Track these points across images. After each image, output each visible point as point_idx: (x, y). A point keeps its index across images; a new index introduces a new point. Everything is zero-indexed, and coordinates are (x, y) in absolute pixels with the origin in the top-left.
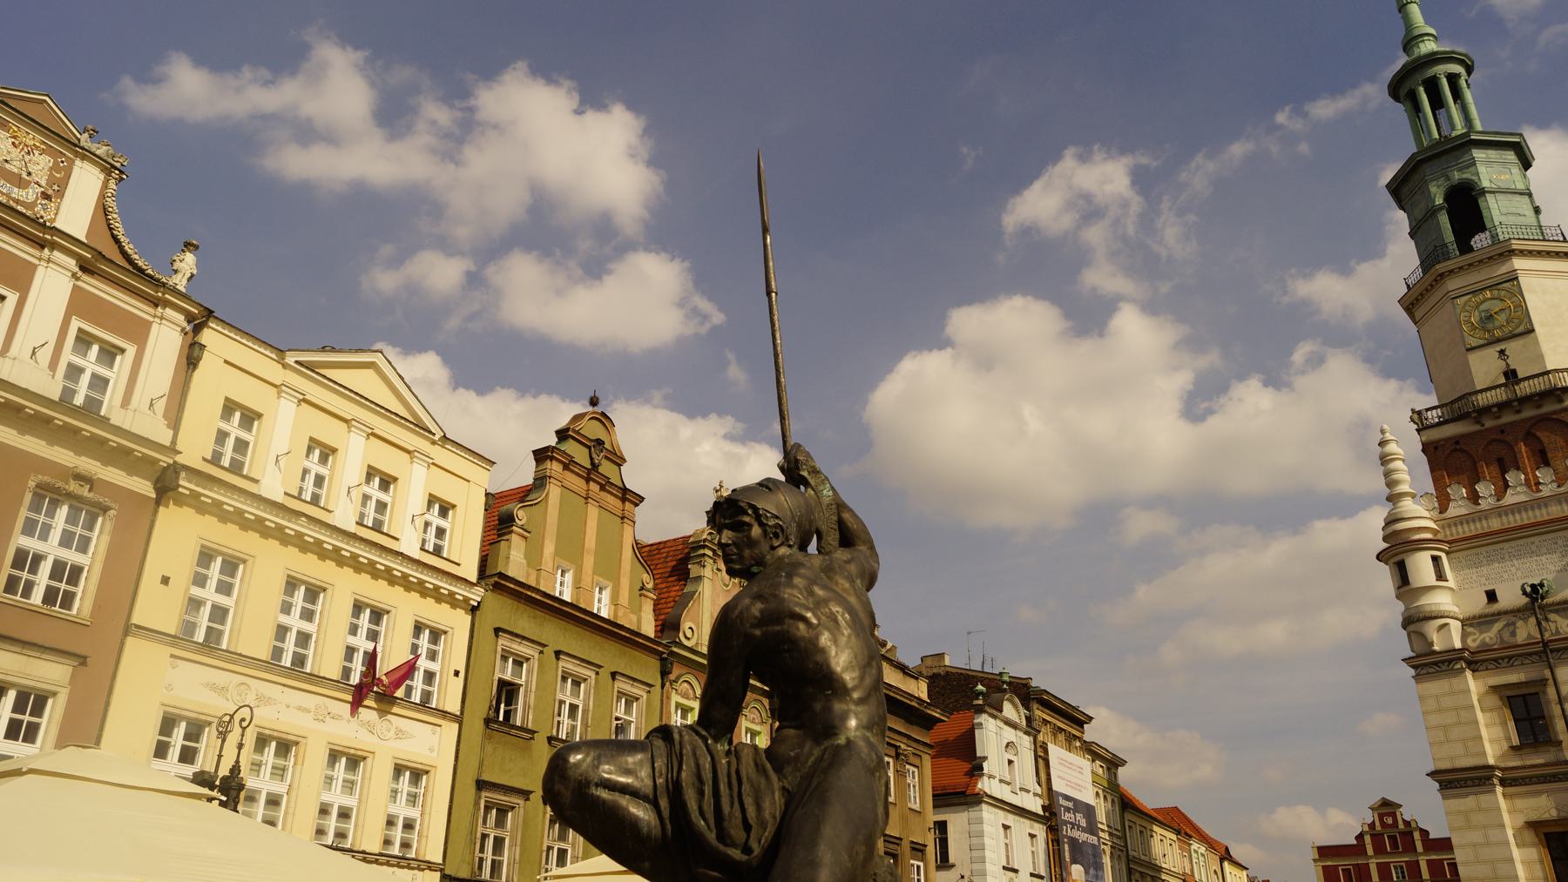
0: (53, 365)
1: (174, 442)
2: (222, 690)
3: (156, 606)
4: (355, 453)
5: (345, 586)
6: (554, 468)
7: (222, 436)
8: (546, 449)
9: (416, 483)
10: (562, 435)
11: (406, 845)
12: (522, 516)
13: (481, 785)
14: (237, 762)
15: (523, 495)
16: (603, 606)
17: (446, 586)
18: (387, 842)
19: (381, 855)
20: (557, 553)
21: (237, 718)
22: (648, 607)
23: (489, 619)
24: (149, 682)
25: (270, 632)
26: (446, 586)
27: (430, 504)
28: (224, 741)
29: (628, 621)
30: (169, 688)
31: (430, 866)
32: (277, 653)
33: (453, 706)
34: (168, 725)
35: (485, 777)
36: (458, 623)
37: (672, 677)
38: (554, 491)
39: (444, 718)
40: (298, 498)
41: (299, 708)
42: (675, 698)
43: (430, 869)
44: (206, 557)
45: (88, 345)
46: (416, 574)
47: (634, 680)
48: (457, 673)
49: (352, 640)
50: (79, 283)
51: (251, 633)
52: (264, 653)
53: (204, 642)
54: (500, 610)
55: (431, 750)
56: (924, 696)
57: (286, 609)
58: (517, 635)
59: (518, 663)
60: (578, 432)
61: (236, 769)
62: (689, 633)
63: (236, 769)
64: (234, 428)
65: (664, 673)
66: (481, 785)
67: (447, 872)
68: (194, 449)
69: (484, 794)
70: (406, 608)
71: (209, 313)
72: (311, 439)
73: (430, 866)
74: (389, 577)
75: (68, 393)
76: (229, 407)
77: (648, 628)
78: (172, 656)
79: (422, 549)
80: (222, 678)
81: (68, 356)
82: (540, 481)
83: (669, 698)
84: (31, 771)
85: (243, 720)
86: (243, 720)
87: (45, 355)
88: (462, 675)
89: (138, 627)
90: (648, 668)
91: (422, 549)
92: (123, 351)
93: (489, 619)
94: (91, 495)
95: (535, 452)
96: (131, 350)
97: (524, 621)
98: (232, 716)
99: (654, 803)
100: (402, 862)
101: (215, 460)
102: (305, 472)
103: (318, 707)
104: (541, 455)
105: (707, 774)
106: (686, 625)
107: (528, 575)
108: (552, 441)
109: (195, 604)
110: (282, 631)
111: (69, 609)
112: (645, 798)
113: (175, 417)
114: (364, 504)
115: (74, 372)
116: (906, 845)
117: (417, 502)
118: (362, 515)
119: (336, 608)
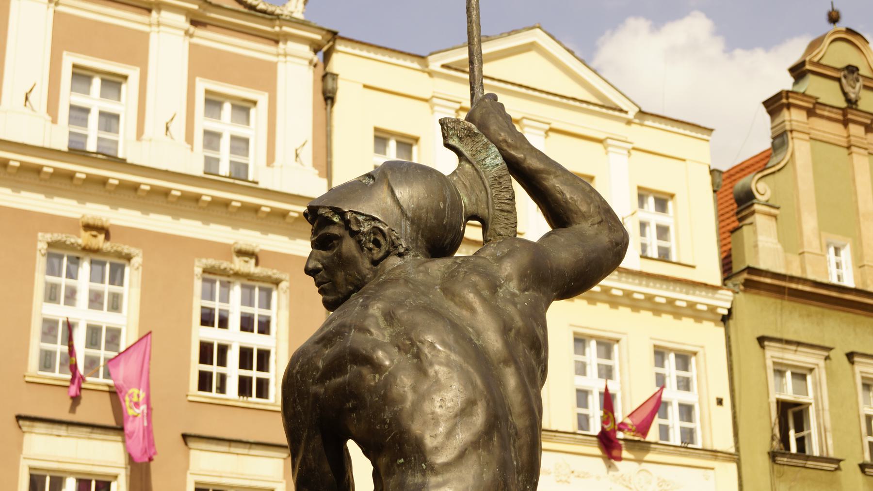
0: (189, 138)
12: (763, 189)
15: (760, 164)
38: (800, 148)
45: (219, 104)
52: (571, 425)
71: (334, 35)
75: (211, 163)
81: (68, 97)
82: (780, 140)
88: (727, 402)
96: (262, 98)
108: (787, 83)
115: (79, 113)
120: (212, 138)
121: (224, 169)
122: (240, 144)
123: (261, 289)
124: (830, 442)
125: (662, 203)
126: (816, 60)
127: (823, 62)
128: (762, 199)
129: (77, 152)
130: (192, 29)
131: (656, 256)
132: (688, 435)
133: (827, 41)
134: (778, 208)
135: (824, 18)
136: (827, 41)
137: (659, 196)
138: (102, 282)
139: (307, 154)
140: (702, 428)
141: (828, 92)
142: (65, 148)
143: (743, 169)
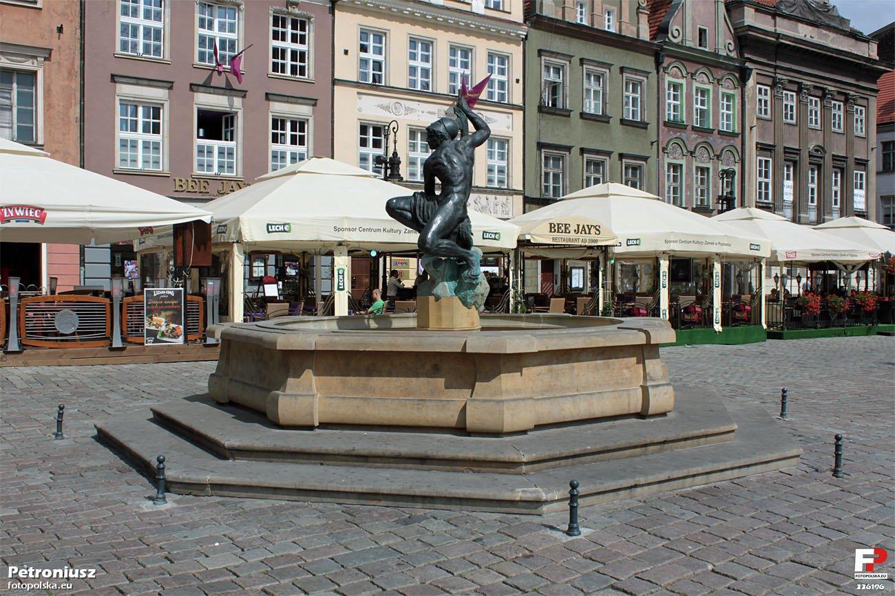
2: (387, 108)
3: (346, 68)
5: (443, 40)
11: (501, 182)
13: (541, 146)
14: (395, 149)
16: (610, 25)
17: (504, 29)
18: (490, 181)
19: (487, 188)
21: (391, 127)
22: (644, 20)
23: (534, 45)
24: (353, 108)
25: (406, 71)
26: (504, 29)
28: (387, 139)
29: (629, 32)
30: (360, 110)
31: (516, 192)
33: (518, 100)
34: (364, 129)
35: (542, 141)
36: (515, 52)
37: (665, 65)
39: (513, 109)
41: (429, 113)
42: (668, 79)
43: (516, 194)
44: (364, 34)
46: (485, 25)
47: (637, 70)
48: (518, 81)
49: (452, 69)
51: (397, 76)
53: (374, 83)
54: (540, 39)
55: (508, 128)
56: (874, 55)
57: (413, 57)
58: (553, 53)
59: (557, 70)
61: (395, 154)
62: (676, 34)
63: (395, 154)
65: (658, 64)
66: (541, 146)
67: (526, 195)
70: (482, 47)
73: (516, 192)
74: (468, 31)
77: (645, 35)
78: (358, 93)
79: (486, 7)
80: (385, 101)
83: (663, 79)
84: (299, 172)
85: (394, 128)
86: (394, 128)
88: (521, 81)
89: (339, 80)
90: (647, 63)
91: (486, 7)
93: (534, 45)
94: (299, 12)
97: (557, 43)
98: (389, 127)
99: (410, 212)
100: (499, 191)
103: (439, 110)
105: (422, 206)
106: (674, 27)
107: (556, 12)
109: (364, 62)
110: (413, 70)
111: (304, 75)
112: (409, 211)
116: (851, 162)
119: (441, 51)
131: (492, 7)
132: (377, 79)
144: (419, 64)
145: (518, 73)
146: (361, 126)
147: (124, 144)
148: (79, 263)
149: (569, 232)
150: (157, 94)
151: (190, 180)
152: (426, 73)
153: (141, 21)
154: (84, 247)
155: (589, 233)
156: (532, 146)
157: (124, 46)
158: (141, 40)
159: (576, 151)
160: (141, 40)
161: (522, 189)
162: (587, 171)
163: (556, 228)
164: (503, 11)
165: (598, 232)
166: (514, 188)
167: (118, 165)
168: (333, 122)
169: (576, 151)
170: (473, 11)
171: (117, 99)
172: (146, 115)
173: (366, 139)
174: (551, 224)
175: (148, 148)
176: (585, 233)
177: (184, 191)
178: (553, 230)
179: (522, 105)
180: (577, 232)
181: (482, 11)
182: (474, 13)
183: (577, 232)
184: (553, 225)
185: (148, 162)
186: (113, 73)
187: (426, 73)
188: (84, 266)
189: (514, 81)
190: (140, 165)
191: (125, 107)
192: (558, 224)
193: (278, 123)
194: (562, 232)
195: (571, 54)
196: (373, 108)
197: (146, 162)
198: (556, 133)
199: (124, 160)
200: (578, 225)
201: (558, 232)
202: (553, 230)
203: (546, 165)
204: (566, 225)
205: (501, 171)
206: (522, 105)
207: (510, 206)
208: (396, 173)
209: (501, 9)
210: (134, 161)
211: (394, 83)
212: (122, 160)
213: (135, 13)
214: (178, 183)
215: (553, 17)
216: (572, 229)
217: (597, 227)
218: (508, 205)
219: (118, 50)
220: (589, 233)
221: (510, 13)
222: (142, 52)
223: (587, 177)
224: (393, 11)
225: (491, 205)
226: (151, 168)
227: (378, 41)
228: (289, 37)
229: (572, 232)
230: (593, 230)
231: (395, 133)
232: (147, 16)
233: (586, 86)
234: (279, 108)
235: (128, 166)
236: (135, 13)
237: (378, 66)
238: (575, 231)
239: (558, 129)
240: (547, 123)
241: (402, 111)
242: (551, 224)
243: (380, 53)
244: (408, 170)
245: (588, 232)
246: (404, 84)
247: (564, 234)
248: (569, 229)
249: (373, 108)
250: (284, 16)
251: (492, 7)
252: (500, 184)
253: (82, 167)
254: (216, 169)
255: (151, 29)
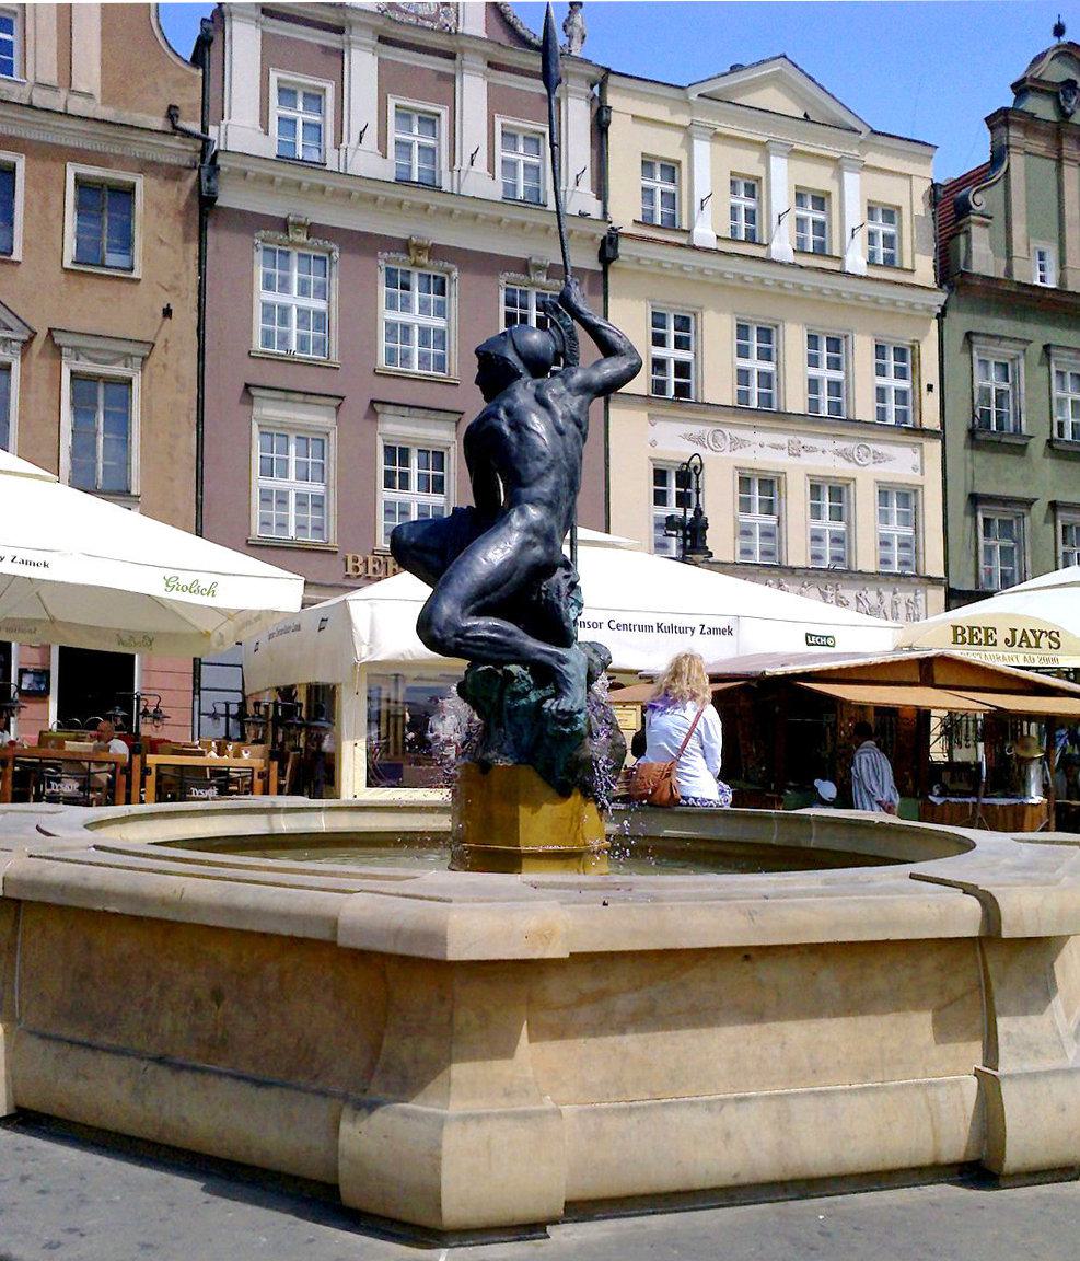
0: (491, 168)
1: (605, 213)
4: (782, 177)
6: (1015, 135)
7: (648, 193)
8: (1004, 111)
9: (854, 193)
10: (1021, 89)
12: (980, 200)
13: (975, 500)
15: (979, 178)
20: (1029, 235)
21: (692, 466)
27: (871, 210)
32: (744, 396)
33: (931, 420)
34: (660, 476)
38: (1016, 162)
40: (734, 240)
45: (409, 117)
48: (930, 388)
50: (491, 80)
52: (729, 398)
57: (743, 352)
60: (1038, 80)
64: (659, 185)
67: (951, 586)
68: (625, 210)
69: (980, 507)
71: (608, 71)
72: (732, 174)
75: (510, 188)
76: (648, 164)
81: (276, 110)
82: (999, 156)
87: (482, 157)
88: (936, 388)
92: (438, 115)
95: (986, 119)
96: (330, 88)
101: (647, 221)
102: (734, 209)
104: (998, 121)
108: (1008, 100)
110: (743, 376)
113: (601, 191)
114: (734, 217)
115: (287, 124)
117: (854, 213)
118: (872, 255)
120: (509, 166)
121: (521, 194)
122: (429, 153)
123: (420, 275)
124: (1023, 422)
125: (751, 191)
126: (1036, 76)
127: (1043, 78)
128: (978, 209)
129: (403, 181)
130: (489, 70)
131: (882, 262)
132: (682, 390)
133: (1049, 56)
134: (990, 218)
135: (1050, 30)
136: (1049, 56)
137: (885, 208)
138: (274, 268)
139: (587, 179)
140: (696, 384)
141: (1042, 108)
142: (500, 199)
143: (966, 180)
144: (754, 364)
145: (930, 373)
146: (655, 470)
147: (266, 498)
148: (192, 688)
149: (995, 644)
150: (317, 417)
151: (371, 558)
152: (835, 387)
153: (293, 300)
154: (201, 663)
155: (1038, 646)
156: (959, 501)
157: (268, 338)
158: (294, 331)
159: (1039, 510)
160: (294, 331)
161: (943, 576)
162: (1064, 543)
163: (967, 635)
164: (901, 269)
165: (1055, 645)
166: (928, 573)
167: (256, 531)
168: (607, 465)
169: (1039, 510)
170: (847, 270)
171: (255, 425)
172: (423, 464)
173: (665, 492)
174: (955, 628)
175: (269, 501)
176: (1029, 646)
177: (359, 576)
178: (960, 639)
179: (939, 429)
180: (1010, 643)
181: (863, 270)
182: (848, 273)
183: (1010, 643)
184: (959, 630)
185: (304, 527)
186: (248, 382)
187: (835, 387)
188: (199, 694)
189: (924, 388)
190: (292, 532)
191: (424, 455)
192: (971, 628)
193: (397, 454)
194: (980, 643)
195: (1028, 338)
196: (674, 440)
197: (300, 527)
198: (1001, 477)
199: (265, 524)
200: (1013, 631)
201: (971, 643)
202: (960, 639)
203: (987, 534)
204: (986, 629)
205: (767, 534)
206: (939, 429)
207: (921, 604)
208: (700, 544)
209: (827, 253)
210: (283, 525)
211: (709, 397)
212: (263, 524)
213: (285, 286)
214: (351, 564)
215: (992, 275)
216: (1001, 636)
217: (1054, 635)
218: (919, 603)
219: (258, 344)
220: (1038, 646)
221: (913, 271)
222: (294, 348)
223: (1064, 553)
224: (863, 301)
225: (887, 603)
226: (310, 538)
227: (764, 339)
228: (671, 341)
229: (1001, 642)
230: (1044, 641)
231: (698, 475)
232: (303, 292)
233: (1056, 393)
234: (394, 428)
235: (273, 534)
236: (285, 286)
237: (682, 369)
238: (1007, 641)
239: (1006, 469)
240: (986, 461)
241: (726, 445)
242: (955, 628)
243: (838, 368)
244: (653, 538)
245: (1033, 644)
246: (729, 398)
247: (982, 647)
248: (995, 637)
249: (674, 440)
250: (523, 288)
251: (882, 262)
252: (904, 567)
253: (199, 533)
254: (292, 532)
255: (309, 312)
